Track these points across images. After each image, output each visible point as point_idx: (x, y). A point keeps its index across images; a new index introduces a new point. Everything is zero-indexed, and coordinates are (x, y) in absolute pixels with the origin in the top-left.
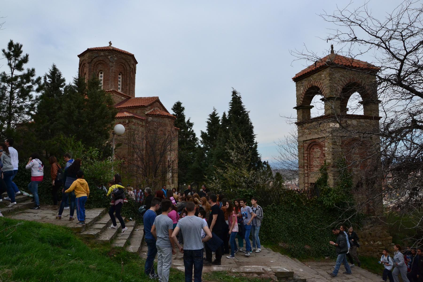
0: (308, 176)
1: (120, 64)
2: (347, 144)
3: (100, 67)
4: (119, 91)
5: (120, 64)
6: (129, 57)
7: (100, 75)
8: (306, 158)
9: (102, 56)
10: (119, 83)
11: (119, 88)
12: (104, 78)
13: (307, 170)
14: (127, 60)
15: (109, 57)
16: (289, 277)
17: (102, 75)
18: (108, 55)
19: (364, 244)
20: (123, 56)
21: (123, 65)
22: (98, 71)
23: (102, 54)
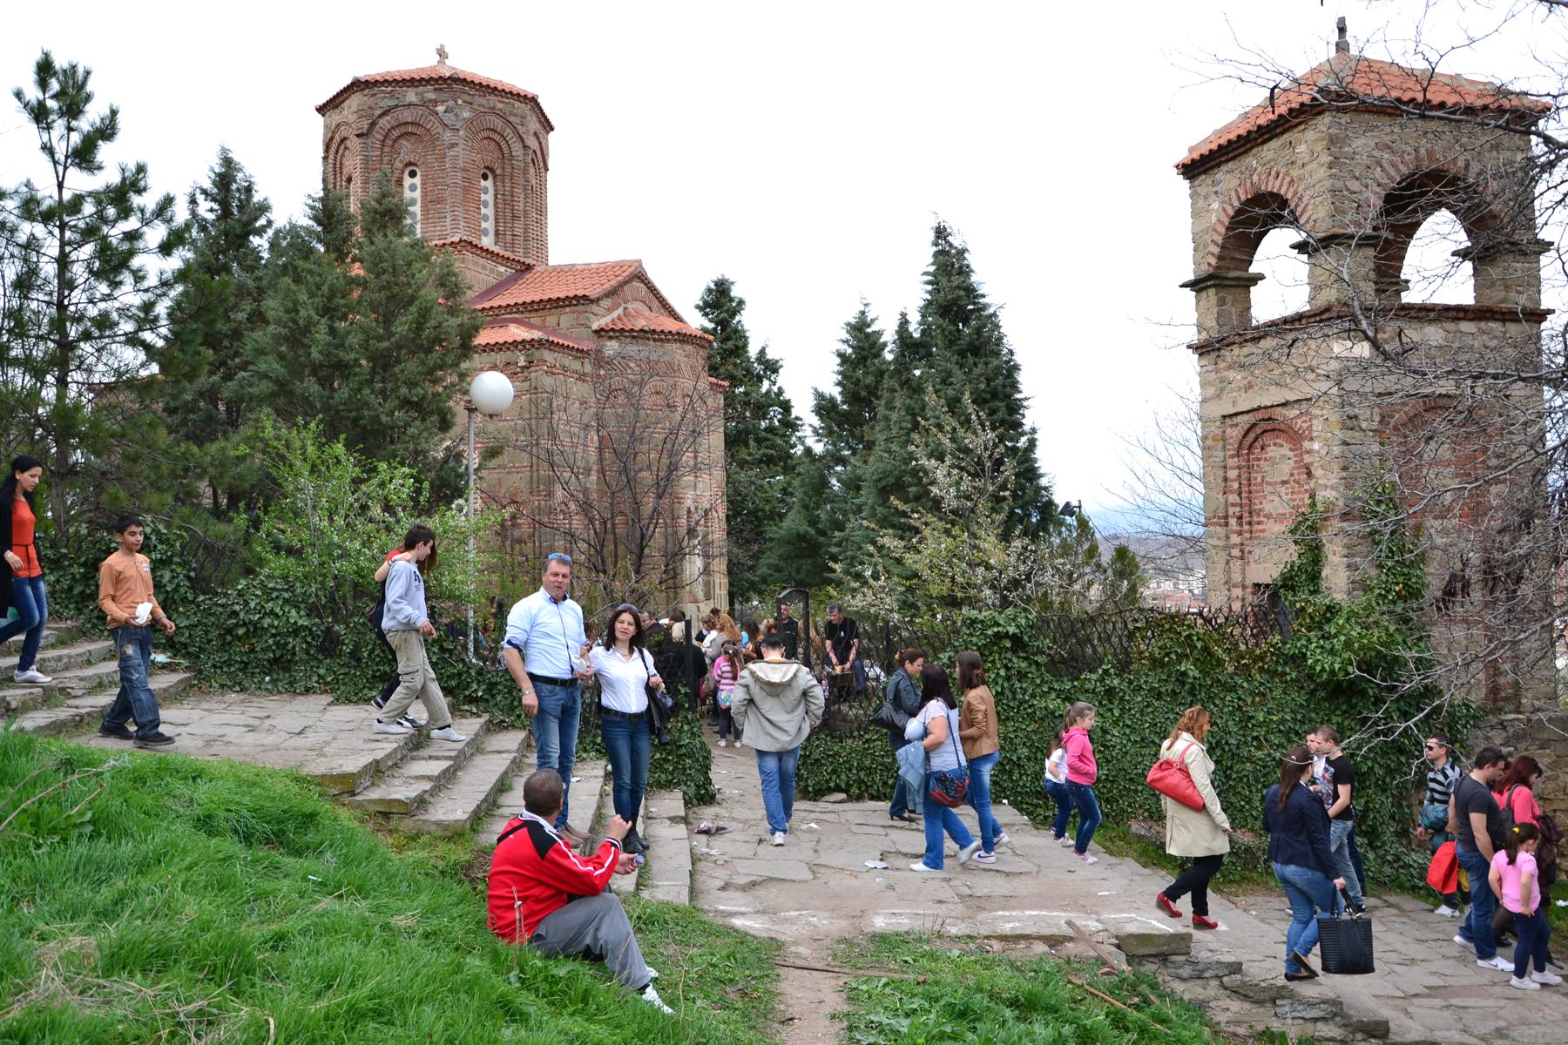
0: (1242, 558)
1: (486, 134)
2: (1404, 425)
3: (407, 150)
4: (487, 242)
5: (486, 134)
6: (517, 104)
7: (408, 181)
8: (1236, 485)
10: (483, 197)
12: (424, 195)
13: (1240, 533)
14: (512, 119)
15: (440, 109)
18: (435, 102)
20: (493, 100)
23: (411, 96)
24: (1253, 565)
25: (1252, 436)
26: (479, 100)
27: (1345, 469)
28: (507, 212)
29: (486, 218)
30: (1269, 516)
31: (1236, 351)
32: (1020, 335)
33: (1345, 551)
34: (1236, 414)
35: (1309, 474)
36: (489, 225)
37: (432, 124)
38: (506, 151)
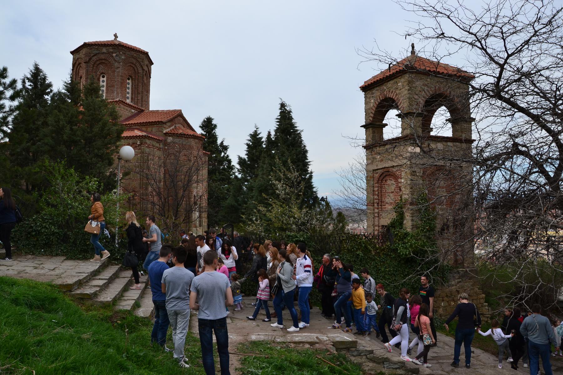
0: (378, 217)
1: (130, 64)
2: (430, 175)
3: (102, 68)
4: (128, 101)
5: (130, 64)
6: (141, 55)
7: (101, 79)
8: (377, 193)
9: (104, 53)
11: (128, 98)
13: (378, 209)
14: (139, 60)
17: (105, 79)
18: (113, 53)
21: (133, 66)
23: (104, 50)
24: (382, 219)
26: (127, 53)
29: (128, 93)
35: (400, 190)
36: (129, 95)
38: (136, 70)
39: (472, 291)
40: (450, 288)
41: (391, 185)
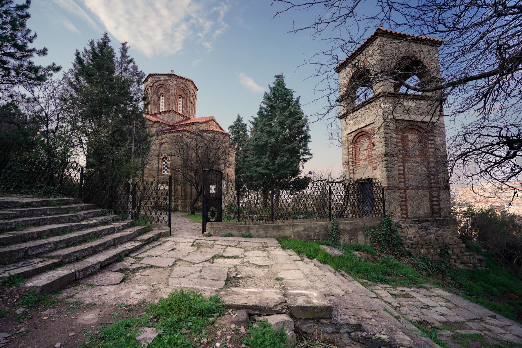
0: (353, 173)
2: (403, 129)
3: (161, 90)
4: (180, 112)
7: (161, 98)
8: (351, 153)
11: (180, 110)
12: (165, 101)
13: (353, 166)
15: (169, 81)
16: (323, 318)
19: (430, 253)
20: (182, 80)
22: (159, 94)
23: (162, 78)
24: (357, 175)
25: (356, 138)
26: (178, 80)
27: (385, 141)
28: (185, 106)
29: (180, 107)
30: (361, 160)
31: (351, 115)
32: (278, 74)
33: (386, 166)
34: (351, 133)
35: (374, 145)
36: (181, 109)
37: (167, 84)
39: (451, 240)
40: (429, 235)
41: (365, 144)
